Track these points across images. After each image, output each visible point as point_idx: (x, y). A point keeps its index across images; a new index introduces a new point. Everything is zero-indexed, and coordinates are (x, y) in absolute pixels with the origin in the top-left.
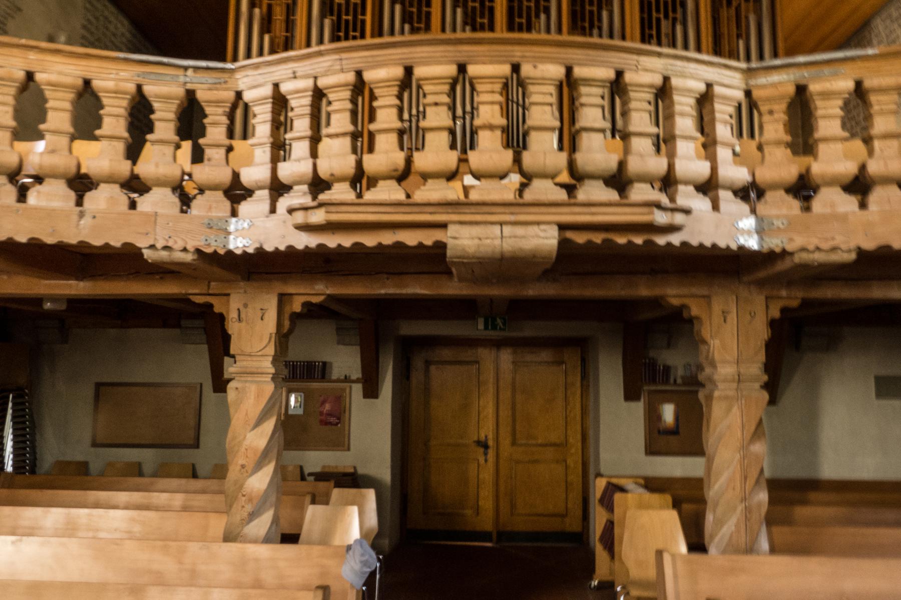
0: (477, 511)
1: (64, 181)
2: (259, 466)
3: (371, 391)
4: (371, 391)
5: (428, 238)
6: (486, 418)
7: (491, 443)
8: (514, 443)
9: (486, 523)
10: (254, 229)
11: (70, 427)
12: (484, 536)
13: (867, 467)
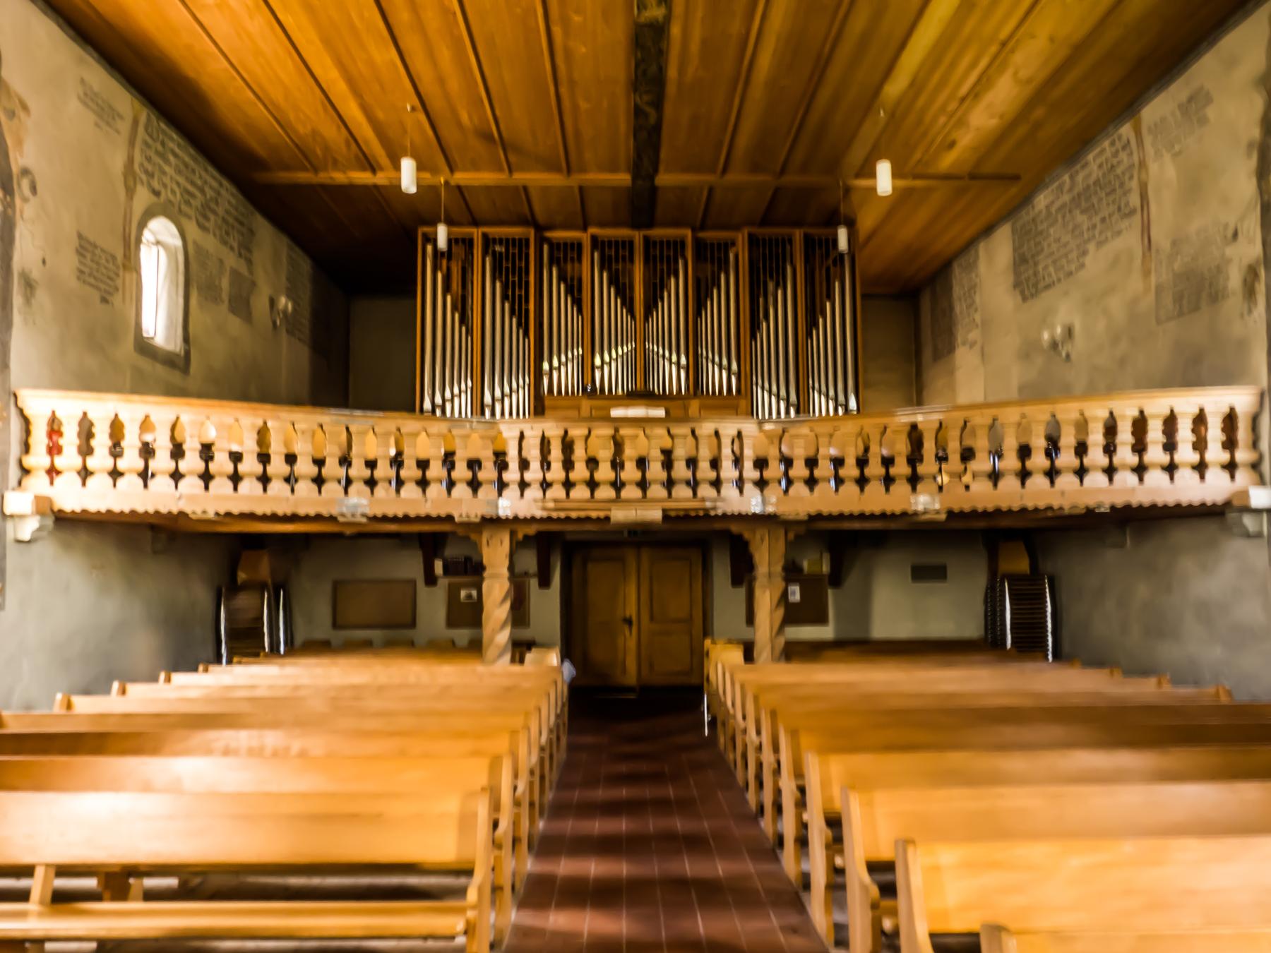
0: (624, 670)
1: (742, 647)
2: (503, 627)
3: (545, 582)
4: (545, 582)
5: (602, 514)
6: (631, 600)
7: (634, 619)
8: (652, 618)
9: (631, 678)
10: (507, 505)
11: (316, 614)
12: (629, 689)
13: (903, 630)
